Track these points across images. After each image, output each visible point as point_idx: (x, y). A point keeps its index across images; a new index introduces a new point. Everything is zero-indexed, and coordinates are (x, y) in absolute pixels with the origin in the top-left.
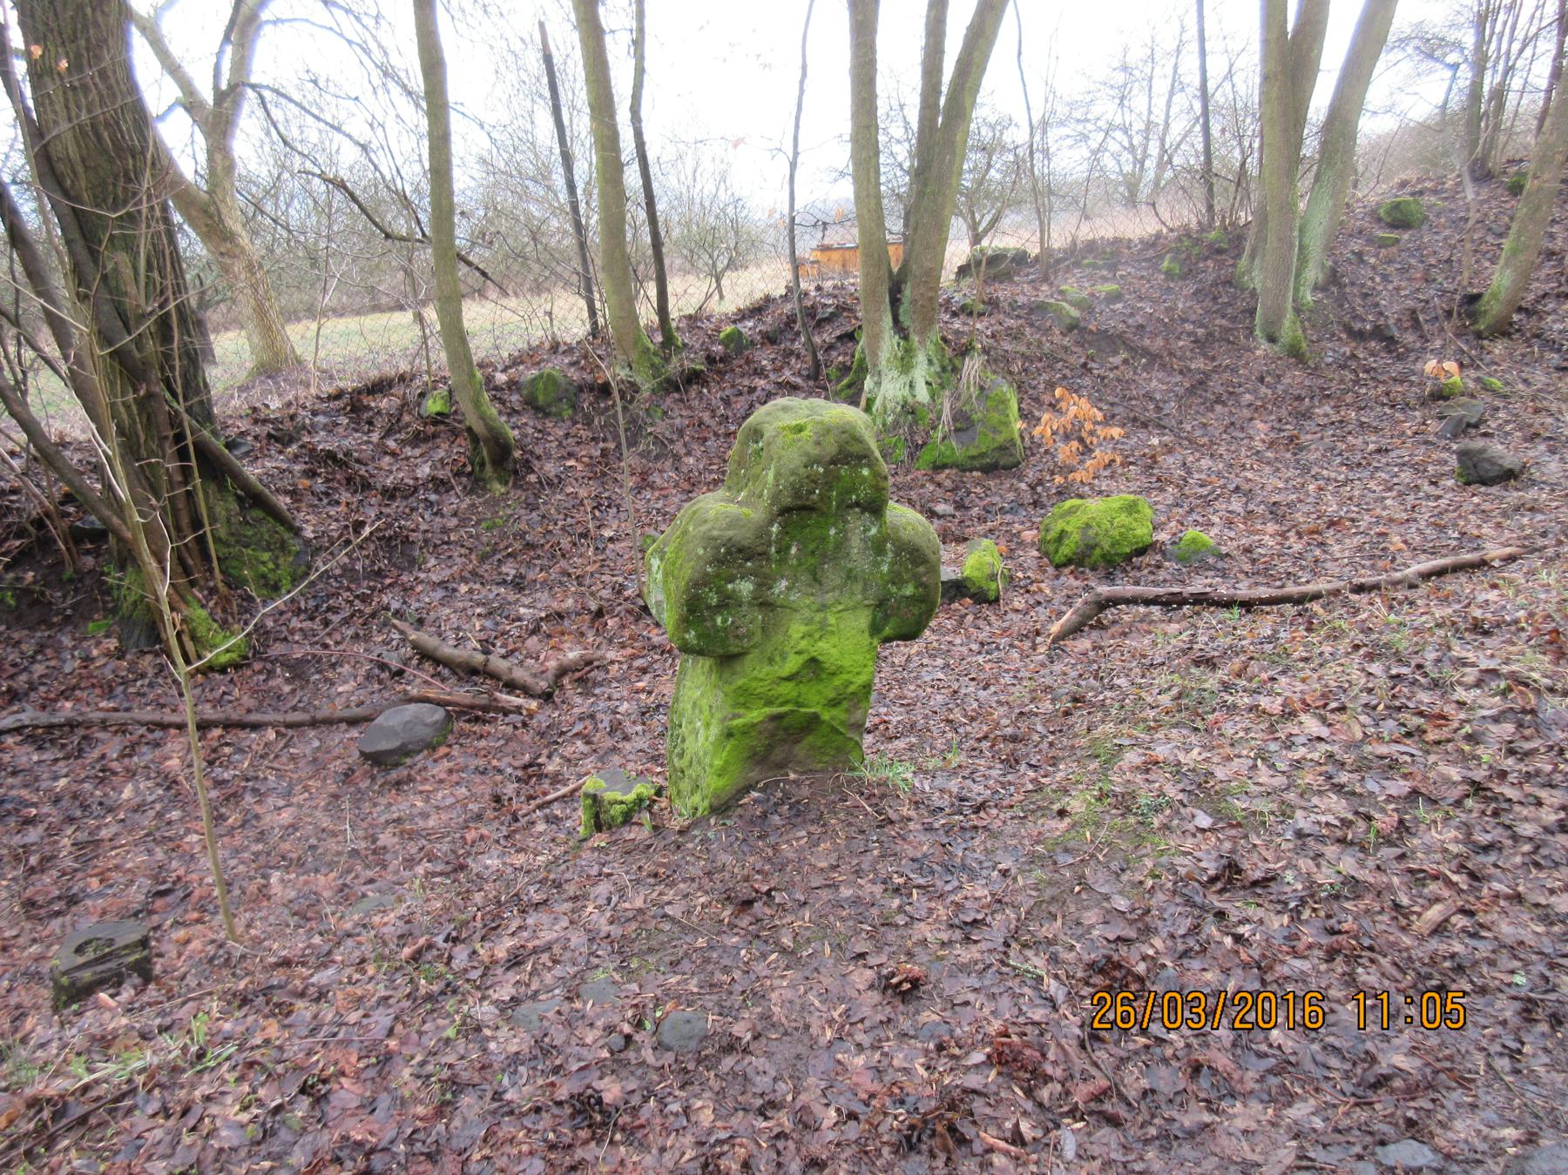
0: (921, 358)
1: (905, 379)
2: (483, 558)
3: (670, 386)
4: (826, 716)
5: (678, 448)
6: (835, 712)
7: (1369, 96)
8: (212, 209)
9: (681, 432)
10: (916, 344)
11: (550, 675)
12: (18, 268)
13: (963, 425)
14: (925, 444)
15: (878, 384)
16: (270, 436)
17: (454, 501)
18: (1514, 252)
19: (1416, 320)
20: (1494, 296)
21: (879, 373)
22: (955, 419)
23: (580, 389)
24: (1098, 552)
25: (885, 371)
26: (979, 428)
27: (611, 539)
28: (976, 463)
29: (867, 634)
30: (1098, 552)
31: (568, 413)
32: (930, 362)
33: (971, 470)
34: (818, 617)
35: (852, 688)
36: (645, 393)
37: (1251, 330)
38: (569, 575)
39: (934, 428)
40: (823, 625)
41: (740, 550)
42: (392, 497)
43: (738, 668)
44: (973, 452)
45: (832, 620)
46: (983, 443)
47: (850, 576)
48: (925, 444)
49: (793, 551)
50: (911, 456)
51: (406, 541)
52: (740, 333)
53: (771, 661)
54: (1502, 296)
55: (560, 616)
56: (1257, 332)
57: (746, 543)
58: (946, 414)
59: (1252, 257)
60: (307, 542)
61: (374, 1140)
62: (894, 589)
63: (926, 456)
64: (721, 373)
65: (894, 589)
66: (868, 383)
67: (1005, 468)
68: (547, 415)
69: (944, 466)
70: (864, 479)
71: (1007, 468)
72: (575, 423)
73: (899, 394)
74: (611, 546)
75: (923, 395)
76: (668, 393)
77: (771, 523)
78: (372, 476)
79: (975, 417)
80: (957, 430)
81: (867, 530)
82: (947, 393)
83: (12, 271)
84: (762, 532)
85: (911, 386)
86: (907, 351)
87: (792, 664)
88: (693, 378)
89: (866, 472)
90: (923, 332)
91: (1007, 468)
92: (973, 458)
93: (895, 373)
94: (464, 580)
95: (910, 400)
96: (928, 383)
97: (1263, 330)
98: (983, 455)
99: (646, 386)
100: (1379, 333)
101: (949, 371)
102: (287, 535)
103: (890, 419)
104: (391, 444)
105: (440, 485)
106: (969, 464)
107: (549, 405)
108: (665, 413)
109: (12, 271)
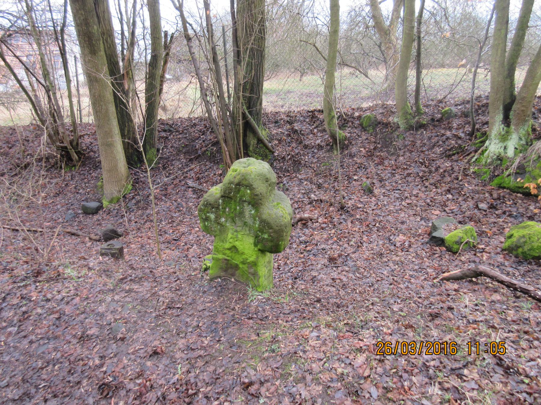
1: (501, 144)
2: (316, 175)
3: (410, 128)
4: (241, 266)
6: (244, 266)
7: (515, 77)
8: (388, 32)
9: (406, 146)
10: (512, 130)
11: (296, 220)
12: (34, 112)
13: (521, 171)
16: (288, 121)
17: (321, 154)
22: (518, 168)
23: (379, 123)
25: (493, 139)
27: (355, 180)
29: (253, 245)
30: (520, 250)
31: (371, 131)
32: (520, 139)
33: (518, 193)
34: (235, 233)
35: (248, 261)
36: (401, 129)
39: (507, 169)
40: (237, 237)
41: (210, 204)
42: (306, 148)
45: (240, 236)
47: (245, 224)
49: (227, 210)
50: (490, 179)
51: (300, 163)
52: (451, 110)
53: (223, 241)
55: (321, 201)
57: (212, 203)
58: (516, 164)
60: (275, 156)
62: (260, 234)
63: (496, 181)
64: (435, 126)
65: (260, 234)
66: (487, 143)
68: (365, 130)
69: (504, 188)
70: (248, 194)
72: (372, 135)
73: (497, 151)
74: (354, 182)
75: (510, 153)
76: (410, 130)
77: (219, 199)
78: (304, 140)
79: (527, 169)
81: (251, 211)
82: (521, 155)
83: (32, 114)
84: (216, 201)
85: (505, 148)
86: (507, 132)
87: (227, 245)
88: (421, 126)
89: (249, 191)
90: (517, 125)
93: (497, 141)
94: (306, 180)
99: (402, 127)
102: (268, 153)
103: (489, 161)
104: (315, 130)
105: (320, 147)
106: (516, 190)
107: (366, 127)
108: (404, 138)
109: (32, 114)
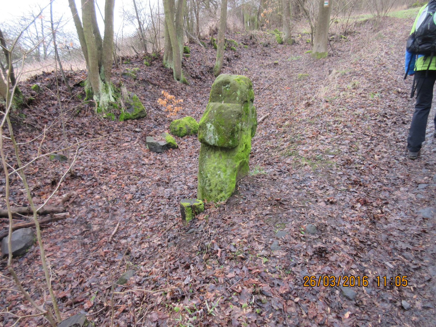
0: (110, 89)
1: (107, 95)
5: (38, 126)
13: (128, 106)
14: (120, 114)
15: (99, 98)
18: (219, 57)
19: (203, 73)
20: (217, 67)
21: (99, 94)
24: (192, 131)
26: (133, 107)
28: (135, 117)
30: (192, 131)
37: (173, 77)
38: (29, 175)
39: (120, 109)
43: (236, 150)
44: (134, 114)
46: (136, 111)
48: (120, 114)
54: (219, 67)
56: (175, 78)
58: (123, 105)
59: (167, 59)
61: (395, 196)
66: (95, 98)
67: (142, 118)
71: (143, 117)
75: (112, 100)
79: (132, 104)
80: (127, 108)
91: (143, 117)
92: (134, 116)
95: (110, 102)
96: (113, 96)
97: (176, 78)
98: (137, 114)
100: (197, 77)
101: (117, 92)
103: (106, 108)
106: (133, 117)
108: (26, 116)
